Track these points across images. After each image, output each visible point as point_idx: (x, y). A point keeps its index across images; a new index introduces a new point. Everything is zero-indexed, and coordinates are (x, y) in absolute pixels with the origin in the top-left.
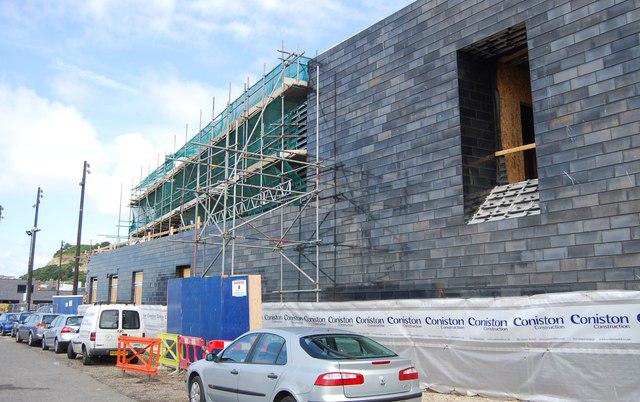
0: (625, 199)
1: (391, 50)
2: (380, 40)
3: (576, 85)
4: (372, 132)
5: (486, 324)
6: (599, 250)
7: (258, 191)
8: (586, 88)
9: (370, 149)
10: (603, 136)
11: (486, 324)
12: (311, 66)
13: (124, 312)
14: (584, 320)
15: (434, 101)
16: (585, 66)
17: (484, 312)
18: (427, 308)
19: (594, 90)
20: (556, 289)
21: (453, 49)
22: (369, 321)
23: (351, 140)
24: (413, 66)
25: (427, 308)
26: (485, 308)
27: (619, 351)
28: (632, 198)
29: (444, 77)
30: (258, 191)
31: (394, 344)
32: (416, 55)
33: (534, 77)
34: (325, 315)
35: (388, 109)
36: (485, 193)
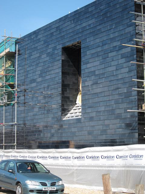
0: (102, 115)
1: (42, 42)
2: (39, 37)
3: (92, 69)
4: (35, 77)
5: (42, 158)
6: (109, 131)
7: (141, 16)
8: (95, 71)
9: (34, 85)
10: (98, 90)
11: (107, 158)
12: (17, 42)
13: (3, 143)
14: (120, 157)
15: (55, 67)
16: (111, 53)
17: (10, 153)
18: (78, 153)
19: (97, 73)
20: (91, 146)
21: (61, 46)
22: (92, 157)
23: (29, 80)
24: (49, 51)
25: (78, 153)
26: (10, 152)
27: (97, 168)
28: (104, 115)
29: (58, 58)
30: (141, 16)
31: (50, 167)
32: (50, 46)
33: (82, 64)
34: (27, 155)
35: (40, 68)
36: (72, 107)
